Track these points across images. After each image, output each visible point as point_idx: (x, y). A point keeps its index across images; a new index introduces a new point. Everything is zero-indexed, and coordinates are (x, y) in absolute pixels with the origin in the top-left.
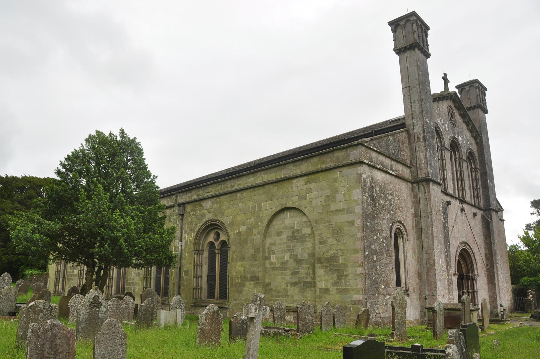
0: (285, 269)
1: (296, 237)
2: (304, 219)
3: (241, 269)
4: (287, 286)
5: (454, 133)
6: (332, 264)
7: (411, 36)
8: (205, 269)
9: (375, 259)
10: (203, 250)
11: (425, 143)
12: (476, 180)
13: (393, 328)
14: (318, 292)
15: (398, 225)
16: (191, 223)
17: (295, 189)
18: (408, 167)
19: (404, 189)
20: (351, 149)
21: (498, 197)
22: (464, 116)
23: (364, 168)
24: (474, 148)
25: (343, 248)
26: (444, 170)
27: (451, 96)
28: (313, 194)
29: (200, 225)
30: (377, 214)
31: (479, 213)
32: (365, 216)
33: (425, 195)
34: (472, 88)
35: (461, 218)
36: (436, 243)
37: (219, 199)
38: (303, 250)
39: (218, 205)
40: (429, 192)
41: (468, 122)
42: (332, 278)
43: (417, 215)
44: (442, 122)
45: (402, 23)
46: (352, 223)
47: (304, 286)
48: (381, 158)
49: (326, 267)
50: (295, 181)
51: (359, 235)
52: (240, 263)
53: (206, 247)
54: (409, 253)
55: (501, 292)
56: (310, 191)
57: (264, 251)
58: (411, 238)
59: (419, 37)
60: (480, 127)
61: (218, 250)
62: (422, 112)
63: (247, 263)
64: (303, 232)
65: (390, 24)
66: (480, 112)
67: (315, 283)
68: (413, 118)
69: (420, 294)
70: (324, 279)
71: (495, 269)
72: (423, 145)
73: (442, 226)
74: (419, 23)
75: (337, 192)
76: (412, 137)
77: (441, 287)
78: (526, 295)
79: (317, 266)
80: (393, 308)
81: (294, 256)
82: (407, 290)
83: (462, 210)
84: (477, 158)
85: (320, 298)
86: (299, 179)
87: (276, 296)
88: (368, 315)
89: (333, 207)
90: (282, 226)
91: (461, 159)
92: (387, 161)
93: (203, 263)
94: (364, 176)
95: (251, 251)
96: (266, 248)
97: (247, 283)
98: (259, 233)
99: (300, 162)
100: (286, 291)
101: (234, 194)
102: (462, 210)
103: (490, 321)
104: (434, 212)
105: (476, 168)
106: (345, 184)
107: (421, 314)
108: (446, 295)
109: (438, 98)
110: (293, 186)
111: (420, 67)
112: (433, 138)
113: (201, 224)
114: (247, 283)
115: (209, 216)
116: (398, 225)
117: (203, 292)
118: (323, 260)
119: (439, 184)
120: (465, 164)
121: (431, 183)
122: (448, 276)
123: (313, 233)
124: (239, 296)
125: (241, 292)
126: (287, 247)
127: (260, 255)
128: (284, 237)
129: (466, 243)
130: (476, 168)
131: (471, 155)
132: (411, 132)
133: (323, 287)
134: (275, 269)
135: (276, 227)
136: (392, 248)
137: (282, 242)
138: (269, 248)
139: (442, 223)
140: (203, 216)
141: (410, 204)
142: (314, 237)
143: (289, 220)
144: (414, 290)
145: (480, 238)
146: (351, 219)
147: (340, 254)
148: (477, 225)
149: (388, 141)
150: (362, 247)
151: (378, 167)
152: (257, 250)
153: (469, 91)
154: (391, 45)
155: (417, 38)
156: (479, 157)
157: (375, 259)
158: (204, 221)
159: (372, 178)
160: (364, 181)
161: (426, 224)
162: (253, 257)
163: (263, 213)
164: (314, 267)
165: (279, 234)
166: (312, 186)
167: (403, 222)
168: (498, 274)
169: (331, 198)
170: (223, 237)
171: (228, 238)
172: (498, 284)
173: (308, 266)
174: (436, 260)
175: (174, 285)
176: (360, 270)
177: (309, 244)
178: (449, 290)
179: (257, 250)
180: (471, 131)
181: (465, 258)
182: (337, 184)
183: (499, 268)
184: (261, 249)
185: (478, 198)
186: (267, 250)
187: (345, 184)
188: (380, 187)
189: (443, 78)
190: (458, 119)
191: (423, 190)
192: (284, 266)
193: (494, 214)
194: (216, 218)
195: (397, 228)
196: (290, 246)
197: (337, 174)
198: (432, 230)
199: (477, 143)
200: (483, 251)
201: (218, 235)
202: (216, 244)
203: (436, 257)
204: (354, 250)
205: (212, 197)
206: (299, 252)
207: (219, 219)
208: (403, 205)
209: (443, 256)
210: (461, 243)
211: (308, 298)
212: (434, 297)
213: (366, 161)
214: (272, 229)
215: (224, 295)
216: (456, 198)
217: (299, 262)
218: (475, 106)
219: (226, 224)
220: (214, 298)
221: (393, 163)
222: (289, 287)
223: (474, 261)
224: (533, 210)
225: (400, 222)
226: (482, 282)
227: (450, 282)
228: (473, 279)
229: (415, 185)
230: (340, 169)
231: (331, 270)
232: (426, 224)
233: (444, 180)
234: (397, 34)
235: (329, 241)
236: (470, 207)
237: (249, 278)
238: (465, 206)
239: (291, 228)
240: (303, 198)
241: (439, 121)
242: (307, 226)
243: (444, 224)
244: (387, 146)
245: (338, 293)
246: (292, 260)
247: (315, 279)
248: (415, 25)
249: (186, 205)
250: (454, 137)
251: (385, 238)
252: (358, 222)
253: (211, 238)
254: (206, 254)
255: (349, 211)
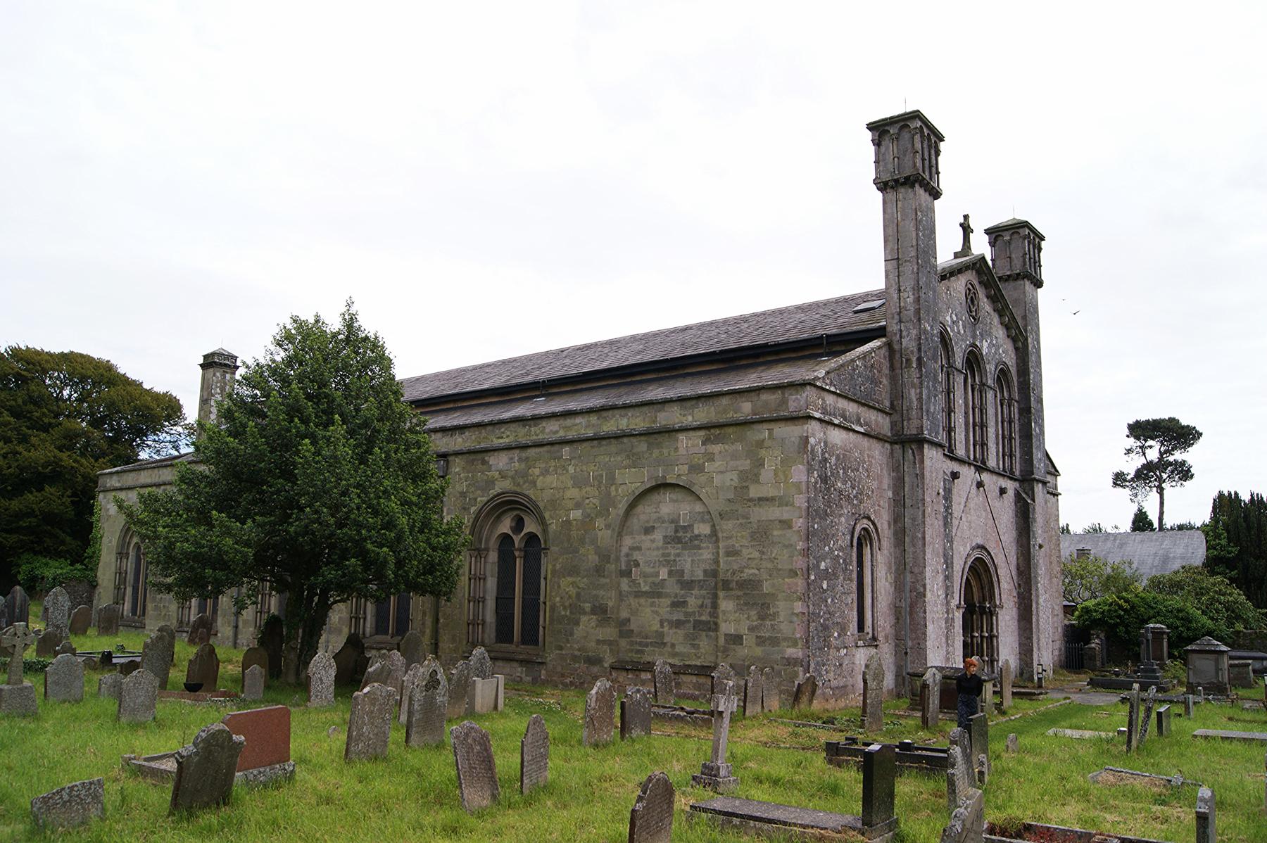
0: (659, 595)
1: (680, 536)
2: (698, 508)
3: (573, 591)
4: (662, 626)
5: (974, 337)
6: (749, 592)
7: (907, 153)
8: (491, 583)
9: (825, 586)
10: (487, 549)
11: (920, 370)
12: (1010, 422)
13: (864, 711)
14: (722, 641)
15: (865, 523)
16: (463, 495)
17: (682, 451)
18: (886, 413)
19: (877, 454)
20: (792, 391)
21: (1049, 447)
22: (997, 299)
23: (814, 425)
24: (1010, 359)
25: (770, 565)
26: (950, 411)
27: (974, 264)
28: (718, 464)
29: (482, 499)
30: (830, 507)
31: (1011, 486)
32: (811, 513)
33: (915, 468)
34: (1016, 236)
35: (977, 499)
36: (928, 556)
37: (524, 454)
38: (694, 564)
39: (523, 466)
40: (922, 462)
41: (1002, 308)
42: (748, 618)
43: (899, 502)
44: (952, 318)
45: (893, 130)
46: (786, 524)
47: (694, 628)
48: (842, 404)
49: (738, 597)
50: (681, 436)
51: (800, 546)
52: (570, 579)
53: (493, 543)
54: (882, 572)
55: (1042, 636)
56: (711, 459)
57: (618, 559)
58: (886, 543)
59: (923, 160)
60: (1024, 317)
61: (520, 550)
62: (918, 312)
63: (583, 582)
64: (696, 532)
65: (872, 127)
66: (1028, 286)
67: (716, 624)
68: (900, 321)
69: (896, 645)
70: (732, 617)
71: (1034, 593)
72: (914, 373)
73: (941, 523)
74: (926, 131)
75: (762, 465)
76: (897, 356)
77: (934, 631)
78: (1088, 641)
79: (721, 594)
80: (865, 681)
81: (677, 574)
82: (874, 638)
83: (980, 485)
84: (1015, 379)
85: (725, 650)
86: (691, 434)
87: (640, 644)
88: (815, 686)
89: (754, 492)
90: (654, 516)
91: (983, 384)
92: (852, 408)
93: (488, 574)
94: (812, 440)
95: (593, 559)
96: (623, 554)
97: (584, 619)
98: (608, 526)
99: (694, 402)
100: (662, 635)
101: (557, 447)
102: (980, 485)
103: (1013, 694)
104: (928, 499)
105: (1011, 399)
106: (777, 453)
107: (896, 680)
108: (943, 651)
109: (949, 274)
110: (679, 445)
111: (921, 221)
112: (935, 359)
113: (485, 499)
114: (584, 619)
115: (502, 486)
116: (865, 523)
117: (487, 631)
118: (733, 585)
119: (940, 446)
120: (990, 395)
121: (926, 446)
122: (947, 612)
123: (714, 533)
124: (568, 641)
125: (572, 634)
126: (663, 555)
127: (612, 567)
128: (658, 536)
129: (982, 547)
130: (1011, 399)
131: (1003, 374)
132: (896, 347)
133: (732, 632)
134: (639, 594)
135: (643, 517)
136: (853, 567)
137: (654, 545)
138: (627, 555)
139: (941, 518)
140: (491, 483)
141: (886, 482)
142: (717, 541)
143: (667, 506)
144: (886, 637)
145: (1008, 534)
146: (786, 517)
147: (765, 576)
148: (1005, 511)
149: (854, 370)
150: (804, 566)
151: (836, 422)
152: (605, 557)
153: (1009, 242)
154: (872, 175)
155: (919, 164)
156: (1019, 376)
157: (825, 586)
158: (493, 492)
159: (826, 443)
160: (813, 450)
161: (914, 520)
162: (597, 571)
163: (617, 490)
164: (715, 596)
165: (648, 530)
166: (716, 448)
167: (873, 517)
168: (1037, 603)
169: (750, 476)
170: (530, 527)
171: (545, 531)
172: (1038, 621)
173: (703, 592)
174: (928, 587)
175: (424, 614)
176: (799, 607)
177: (706, 554)
178: (947, 638)
179: (605, 557)
180: (1007, 327)
181: (980, 574)
182: (763, 452)
183: (1041, 591)
184: (613, 556)
185: (1011, 456)
186: (623, 559)
187: (777, 453)
188: (838, 458)
189: (961, 225)
190: (985, 305)
191: (911, 457)
192: (656, 593)
193: (1038, 488)
194: (518, 490)
195: (864, 529)
196: (669, 555)
197: (763, 432)
198: (924, 532)
199: (1016, 349)
200: (1013, 560)
201: (519, 524)
202: (517, 539)
203: (928, 581)
204: (791, 570)
205: (509, 448)
206: (688, 567)
207: (526, 493)
208: (875, 485)
209: (941, 578)
210: (973, 549)
211: (703, 651)
212: (921, 652)
213: (817, 415)
214: (635, 521)
215: (531, 636)
216: (970, 464)
217: (688, 585)
218: (1018, 274)
219: (541, 505)
220: (511, 642)
221: (862, 410)
222: (666, 629)
223: (995, 579)
224: (1132, 442)
225: (869, 518)
226: (1007, 618)
227: (949, 622)
228: (991, 614)
229: (897, 446)
230: (771, 426)
231: (745, 604)
232: (914, 520)
233: (950, 430)
234: (883, 149)
235: (745, 551)
236: (995, 477)
237: (588, 610)
238: (985, 477)
239: (672, 522)
240: (697, 469)
241: (948, 318)
242: (703, 521)
243: (946, 518)
244: (852, 378)
245: (758, 645)
246: (673, 580)
247: (717, 617)
248: (917, 137)
249: (450, 458)
250: (974, 345)
251: (841, 549)
252: (799, 523)
253: (505, 526)
254: (493, 556)
255: (783, 502)
